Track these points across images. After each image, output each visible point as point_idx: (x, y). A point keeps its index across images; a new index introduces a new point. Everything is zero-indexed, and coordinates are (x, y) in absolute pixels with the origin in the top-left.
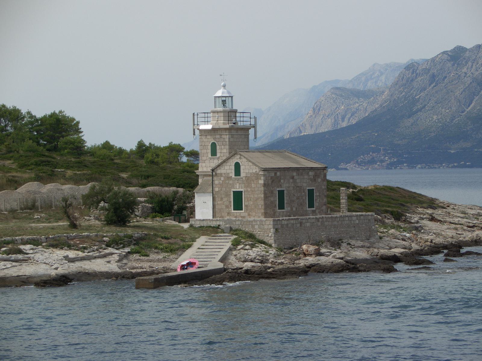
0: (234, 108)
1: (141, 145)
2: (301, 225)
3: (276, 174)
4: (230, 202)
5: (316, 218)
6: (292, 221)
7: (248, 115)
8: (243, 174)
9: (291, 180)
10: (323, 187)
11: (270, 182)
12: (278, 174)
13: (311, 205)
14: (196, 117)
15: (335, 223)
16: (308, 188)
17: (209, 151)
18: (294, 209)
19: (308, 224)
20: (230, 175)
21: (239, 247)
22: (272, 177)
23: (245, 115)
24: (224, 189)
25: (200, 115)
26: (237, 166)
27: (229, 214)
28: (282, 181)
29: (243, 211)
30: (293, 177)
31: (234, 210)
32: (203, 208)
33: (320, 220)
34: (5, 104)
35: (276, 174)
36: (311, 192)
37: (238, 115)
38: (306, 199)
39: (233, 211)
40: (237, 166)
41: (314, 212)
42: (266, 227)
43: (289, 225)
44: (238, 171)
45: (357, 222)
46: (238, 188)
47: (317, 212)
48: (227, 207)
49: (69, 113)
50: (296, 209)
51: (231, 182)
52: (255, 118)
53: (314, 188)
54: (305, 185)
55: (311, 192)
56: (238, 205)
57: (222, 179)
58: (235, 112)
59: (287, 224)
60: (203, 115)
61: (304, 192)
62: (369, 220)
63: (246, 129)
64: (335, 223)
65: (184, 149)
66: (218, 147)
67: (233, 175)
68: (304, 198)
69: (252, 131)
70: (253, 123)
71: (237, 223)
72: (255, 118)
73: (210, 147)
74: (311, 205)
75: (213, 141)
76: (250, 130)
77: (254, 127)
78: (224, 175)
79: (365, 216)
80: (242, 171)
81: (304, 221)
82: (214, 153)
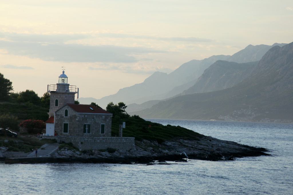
0: (68, 83)
1: (138, 116)
2: (94, 141)
3: (85, 116)
4: (62, 128)
5: (103, 138)
6: (90, 139)
7: (75, 87)
8: (69, 115)
9: (93, 120)
10: (110, 124)
11: (81, 120)
12: (86, 116)
13: (103, 132)
14: (49, 86)
15: (113, 141)
16: (101, 124)
17: (55, 104)
18: (94, 133)
19: (99, 141)
20: (63, 115)
21: (62, 149)
22: (82, 117)
23: (73, 87)
24: (60, 122)
25: (51, 86)
26: (66, 111)
27: (61, 134)
28: (88, 120)
29: (68, 133)
30: (94, 118)
31: (64, 132)
32: (50, 130)
33: (105, 139)
34: (28, 90)
35: (85, 116)
36: (103, 126)
37: (69, 86)
38: (100, 129)
39: (63, 133)
40: (66, 111)
41: (104, 136)
42: (77, 141)
43: (89, 141)
44: (66, 115)
45: (125, 141)
46: (66, 122)
47: (106, 135)
48: (61, 131)
49: (30, 89)
50: (95, 133)
51: (63, 119)
52: (78, 89)
53: (105, 124)
54: (100, 122)
55: (103, 126)
56: (66, 130)
57: (59, 117)
58: (68, 85)
59: (87, 140)
60: (53, 86)
61: (99, 125)
62: (131, 141)
63: (73, 94)
64: (113, 141)
65: (130, 116)
66: (59, 102)
67: (64, 115)
68: (99, 128)
69: (76, 95)
70: (77, 91)
71: (64, 138)
72: (78, 89)
73: (55, 101)
74: (103, 132)
75: (57, 99)
76: (75, 94)
77: (78, 93)
78: (60, 115)
79: (48, 137)
80: (68, 114)
81: (96, 139)
82: (57, 105)
